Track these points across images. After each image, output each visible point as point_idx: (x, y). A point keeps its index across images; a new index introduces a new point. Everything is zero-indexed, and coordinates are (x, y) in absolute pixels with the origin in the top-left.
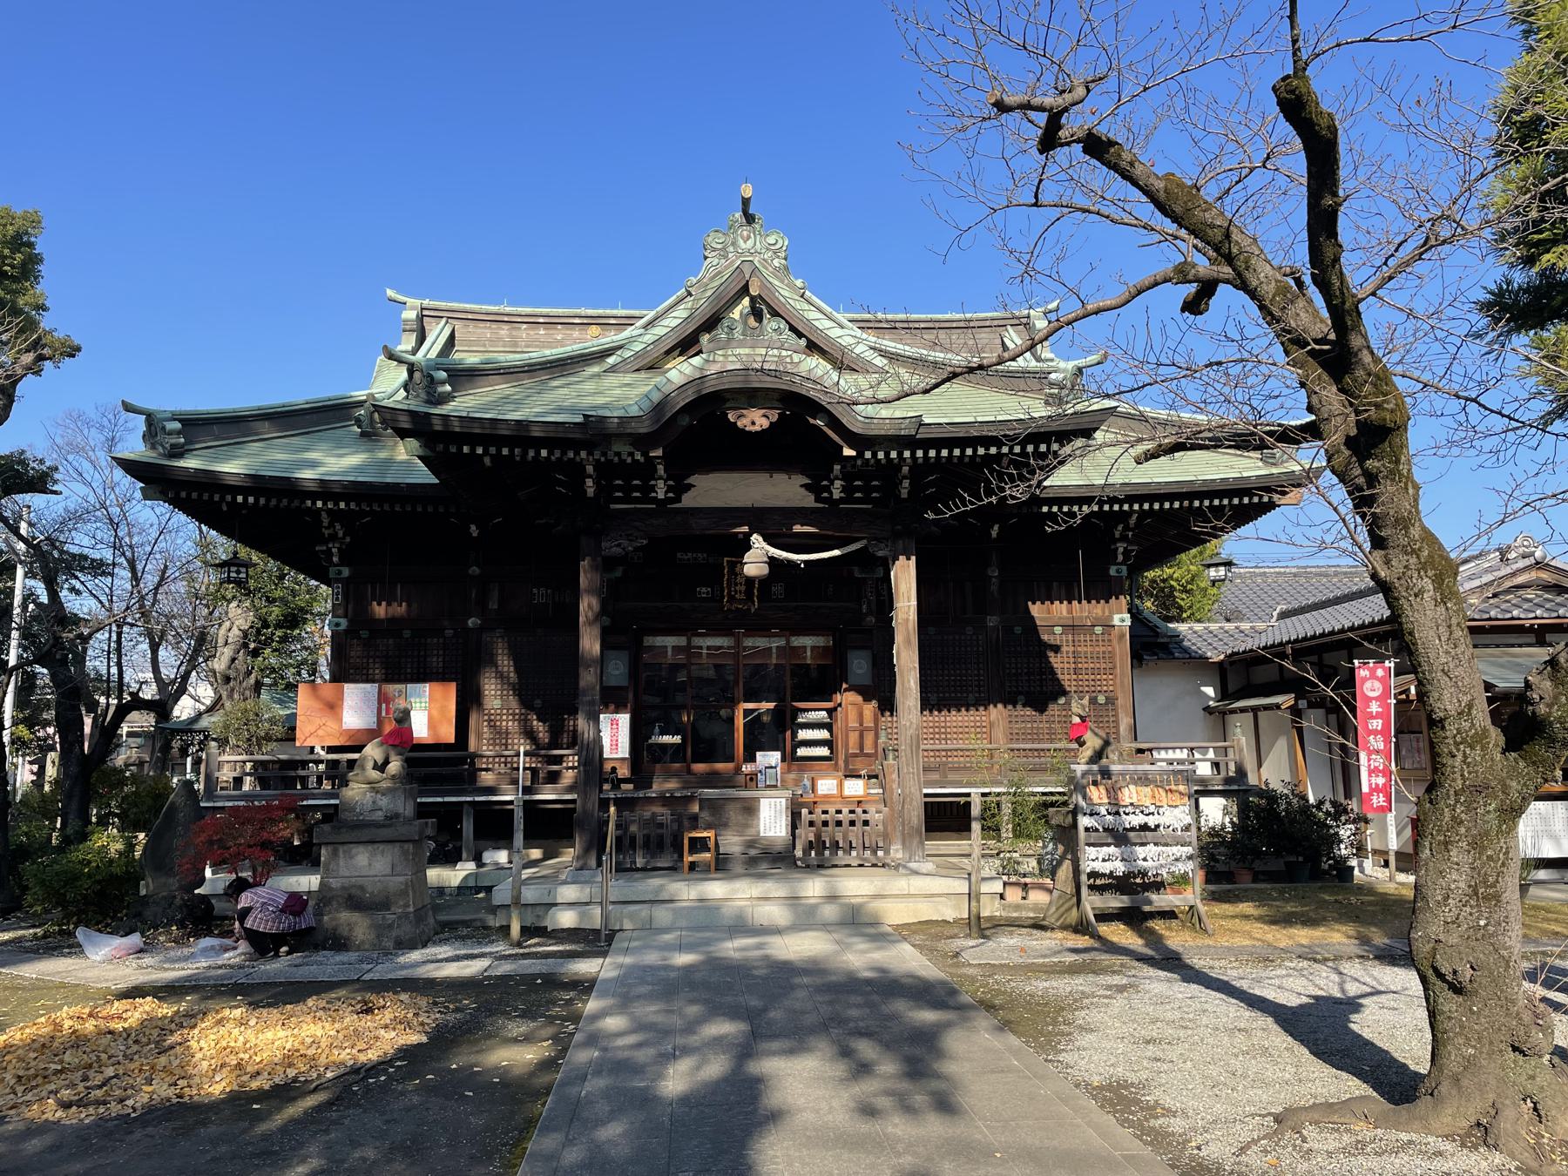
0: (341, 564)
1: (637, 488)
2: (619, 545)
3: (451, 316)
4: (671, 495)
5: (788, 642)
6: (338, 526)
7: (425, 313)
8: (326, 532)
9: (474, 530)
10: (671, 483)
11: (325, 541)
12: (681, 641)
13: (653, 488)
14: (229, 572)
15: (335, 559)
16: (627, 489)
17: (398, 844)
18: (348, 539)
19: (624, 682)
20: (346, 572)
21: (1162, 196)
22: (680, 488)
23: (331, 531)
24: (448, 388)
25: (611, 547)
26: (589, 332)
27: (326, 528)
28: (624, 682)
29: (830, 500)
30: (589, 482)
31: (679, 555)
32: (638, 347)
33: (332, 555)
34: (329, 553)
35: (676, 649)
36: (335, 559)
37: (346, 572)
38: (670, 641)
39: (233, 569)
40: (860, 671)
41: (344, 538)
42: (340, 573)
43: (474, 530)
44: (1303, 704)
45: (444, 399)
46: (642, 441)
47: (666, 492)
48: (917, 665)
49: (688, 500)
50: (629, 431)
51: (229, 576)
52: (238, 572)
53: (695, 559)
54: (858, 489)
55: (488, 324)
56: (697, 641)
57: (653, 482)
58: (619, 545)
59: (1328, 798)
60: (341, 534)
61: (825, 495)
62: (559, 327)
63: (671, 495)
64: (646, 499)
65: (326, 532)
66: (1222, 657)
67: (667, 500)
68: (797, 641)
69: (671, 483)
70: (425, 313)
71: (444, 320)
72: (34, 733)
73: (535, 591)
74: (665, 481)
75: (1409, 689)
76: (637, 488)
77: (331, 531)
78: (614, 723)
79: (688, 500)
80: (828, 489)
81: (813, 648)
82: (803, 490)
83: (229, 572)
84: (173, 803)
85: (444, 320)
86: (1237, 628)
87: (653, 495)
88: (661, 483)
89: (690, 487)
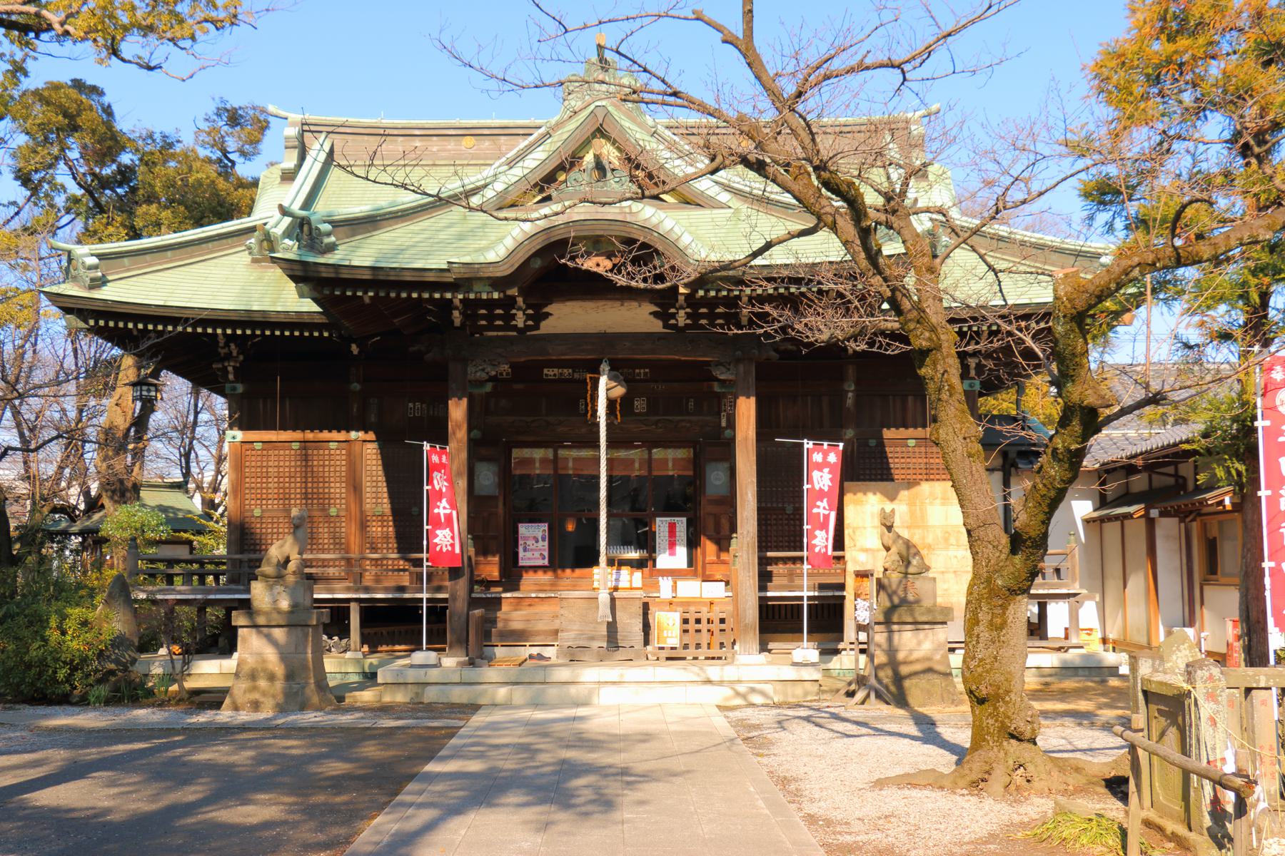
0: (237, 380)
1: (499, 317)
2: (483, 370)
3: (333, 130)
4: (530, 323)
5: (650, 453)
6: (233, 346)
7: (306, 128)
8: (222, 351)
9: (355, 349)
10: (530, 312)
11: (222, 360)
12: (550, 453)
13: (513, 317)
14: (141, 390)
15: (231, 377)
16: (491, 318)
17: (299, 628)
18: (241, 358)
19: (493, 491)
20: (240, 388)
21: (797, 194)
22: (539, 317)
23: (226, 350)
24: (333, 239)
25: (477, 371)
26: (464, 143)
27: (223, 348)
28: (493, 491)
29: (675, 327)
30: (456, 313)
31: (545, 371)
32: (499, 186)
33: (228, 372)
34: (225, 371)
35: (544, 461)
36: (231, 377)
37: (240, 388)
38: (538, 454)
39: (145, 388)
40: (718, 483)
41: (237, 357)
42: (234, 389)
43: (355, 349)
44: (1154, 513)
45: (331, 248)
46: (497, 283)
47: (525, 321)
48: (755, 480)
49: (546, 327)
50: (487, 275)
51: (141, 395)
52: (149, 391)
53: (561, 374)
54: (703, 316)
55: (366, 138)
56: (563, 453)
57: (514, 311)
58: (483, 370)
59: (876, 576)
60: (235, 353)
61: (673, 322)
62: (435, 138)
63: (530, 323)
64: (508, 327)
65: (222, 351)
66: (1097, 466)
67: (527, 328)
68: (658, 453)
69: (530, 312)
70: (306, 128)
71: (323, 135)
72: (81, 533)
73: (411, 405)
74: (524, 311)
75: (1223, 500)
76: (499, 317)
77: (226, 350)
78: (672, 527)
79: (546, 327)
80: (673, 316)
81: (674, 460)
82: (651, 317)
83: (141, 390)
84: (445, 514)
85: (323, 135)
86: (1124, 435)
87: (514, 323)
88: (520, 314)
89: (548, 315)
